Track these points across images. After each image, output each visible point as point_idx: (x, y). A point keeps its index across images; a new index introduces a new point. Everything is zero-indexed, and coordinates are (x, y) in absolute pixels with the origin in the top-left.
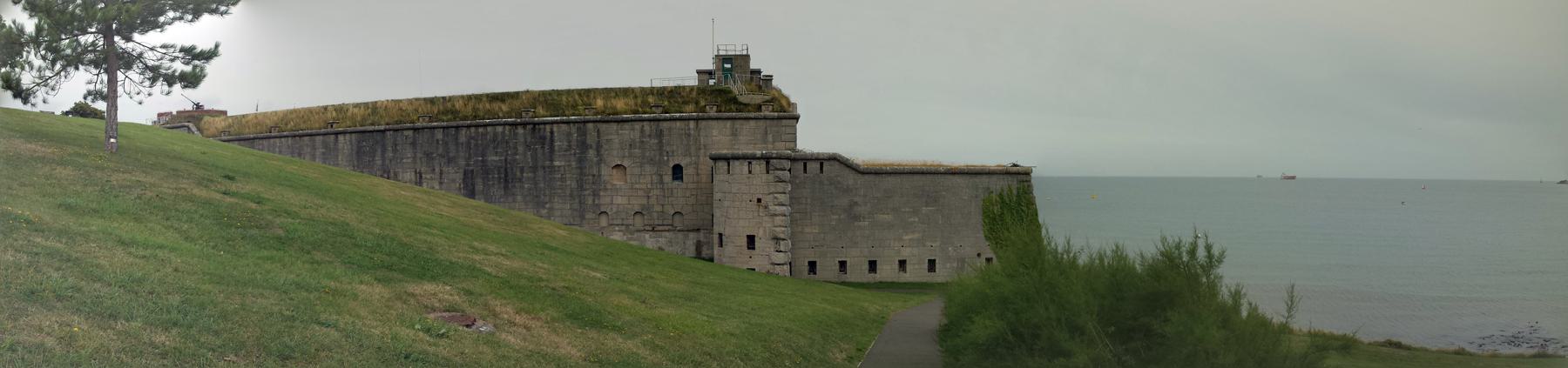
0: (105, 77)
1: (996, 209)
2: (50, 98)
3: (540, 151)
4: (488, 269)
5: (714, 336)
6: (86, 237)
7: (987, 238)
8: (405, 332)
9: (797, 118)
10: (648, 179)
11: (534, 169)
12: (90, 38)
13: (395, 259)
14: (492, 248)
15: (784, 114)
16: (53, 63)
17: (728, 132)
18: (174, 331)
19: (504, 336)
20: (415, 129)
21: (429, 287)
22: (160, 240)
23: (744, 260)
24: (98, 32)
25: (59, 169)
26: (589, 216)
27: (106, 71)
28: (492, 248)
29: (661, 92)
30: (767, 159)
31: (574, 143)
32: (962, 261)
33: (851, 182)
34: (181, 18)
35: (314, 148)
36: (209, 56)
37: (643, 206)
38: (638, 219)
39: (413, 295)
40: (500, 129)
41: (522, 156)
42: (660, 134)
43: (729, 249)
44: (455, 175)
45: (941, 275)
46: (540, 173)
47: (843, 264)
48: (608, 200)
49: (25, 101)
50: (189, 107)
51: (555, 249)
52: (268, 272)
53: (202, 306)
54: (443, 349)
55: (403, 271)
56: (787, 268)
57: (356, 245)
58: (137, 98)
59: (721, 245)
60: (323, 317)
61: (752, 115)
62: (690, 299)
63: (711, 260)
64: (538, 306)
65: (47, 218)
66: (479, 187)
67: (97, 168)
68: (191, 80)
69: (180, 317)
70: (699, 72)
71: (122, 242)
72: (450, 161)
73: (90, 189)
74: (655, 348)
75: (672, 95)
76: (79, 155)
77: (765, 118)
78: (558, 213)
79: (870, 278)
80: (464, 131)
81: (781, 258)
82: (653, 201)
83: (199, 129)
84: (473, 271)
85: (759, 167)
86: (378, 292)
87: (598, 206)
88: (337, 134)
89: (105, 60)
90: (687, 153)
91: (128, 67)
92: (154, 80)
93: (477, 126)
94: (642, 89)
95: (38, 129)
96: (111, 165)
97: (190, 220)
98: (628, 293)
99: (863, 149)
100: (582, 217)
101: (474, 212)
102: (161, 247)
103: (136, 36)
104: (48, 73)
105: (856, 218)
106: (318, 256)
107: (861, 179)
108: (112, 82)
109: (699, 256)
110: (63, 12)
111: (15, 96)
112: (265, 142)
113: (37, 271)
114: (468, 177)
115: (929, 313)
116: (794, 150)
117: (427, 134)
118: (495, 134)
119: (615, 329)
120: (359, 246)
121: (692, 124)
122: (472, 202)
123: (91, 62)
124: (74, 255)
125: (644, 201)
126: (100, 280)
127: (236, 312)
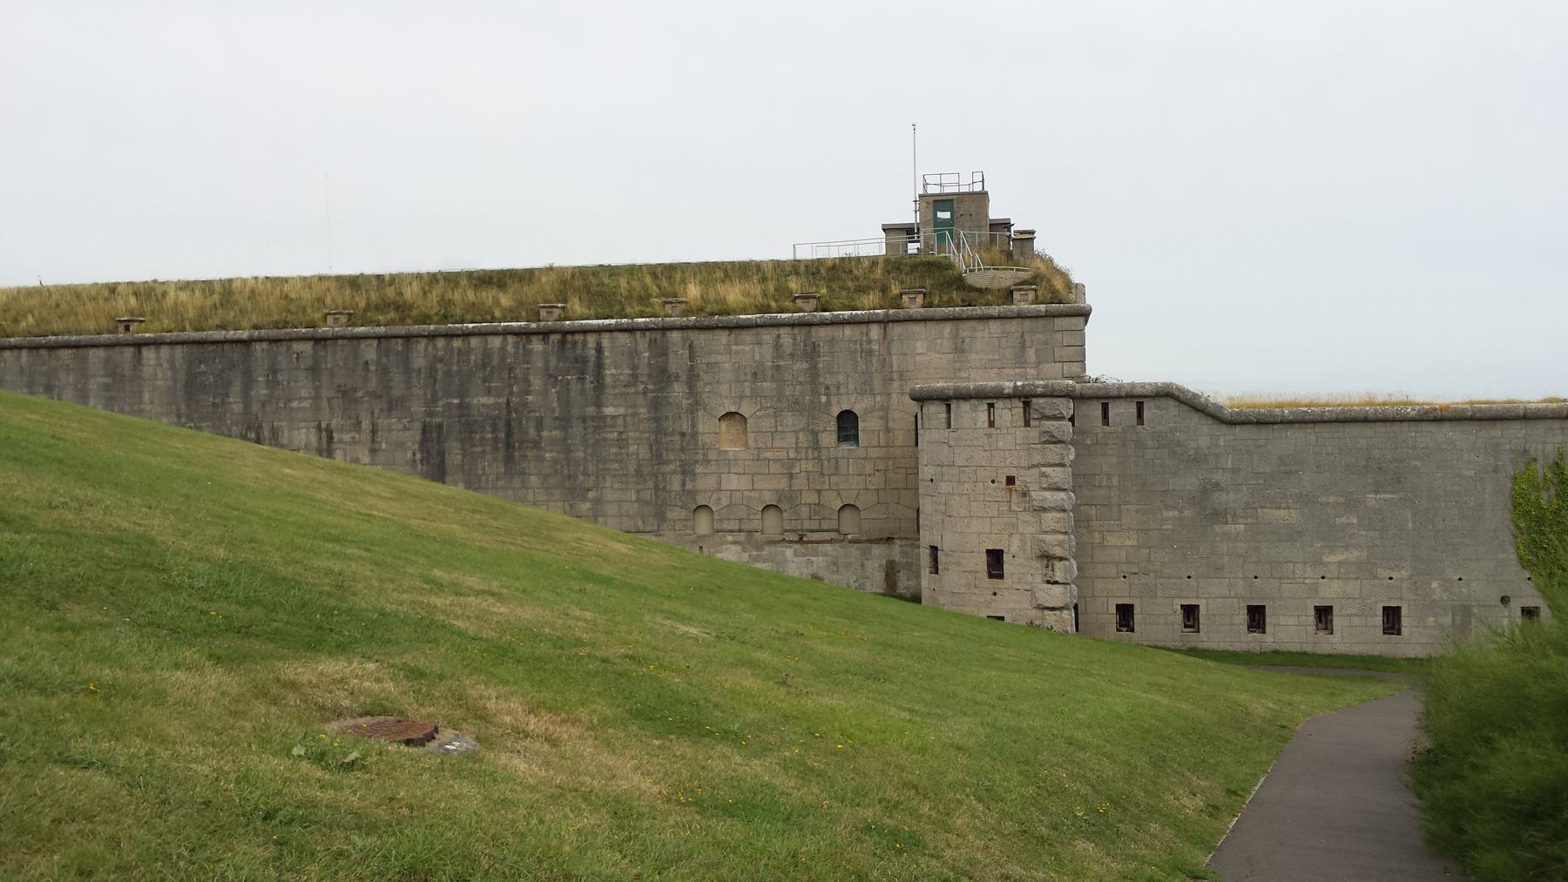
1: (1546, 498)
3: (575, 387)
5: (922, 750)
7: (1524, 563)
8: (271, 765)
9: (1085, 314)
11: (564, 422)
13: (257, 611)
14: (473, 581)
15: (1059, 306)
17: (947, 345)
19: (504, 759)
20: (318, 340)
21: (331, 666)
23: (982, 599)
26: (674, 514)
29: (813, 270)
30: (1025, 398)
31: (643, 370)
32: (1464, 612)
33: (1204, 442)
35: (84, 374)
38: (771, 519)
39: (293, 685)
40: (496, 342)
41: (539, 395)
42: (812, 352)
43: (952, 577)
44: (402, 433)
45: (1414, 640)
46: (577, 429)
47: (1190, 612)
48: (711, 482)
51: (608, 582)
54: (352, 794)
55: (274, 636)
56: (1068, 616)
57: (167, 586)
60: (76, 748)
61: (994, 310)
63: (916, 599)
66: (454, 458)
72: (393, 405)
74: (806, 773)
75: (834, 277)
77: (1021, 316)
78: (612, 509)
79: (1250, 641)
81: (1056, 596)
82: (800, 483)
84: (428, 629)
85: (1009, 414)
88: (139, 345)
90: (866, 389)
93: (450, 336)
94: (777, 265)
99: (1227, 374)
100: (661, 517)
101: (444, 508)
105: (1218, 516)
106: (75, 613)
107: (1226, 436)
109: (891, 590)
115: (1392, 724)
116: (1080, 378)
117: (342, 350)
118: (487, 354)
119: (732, 738)
121: (875, 331)
125: (783, 484)
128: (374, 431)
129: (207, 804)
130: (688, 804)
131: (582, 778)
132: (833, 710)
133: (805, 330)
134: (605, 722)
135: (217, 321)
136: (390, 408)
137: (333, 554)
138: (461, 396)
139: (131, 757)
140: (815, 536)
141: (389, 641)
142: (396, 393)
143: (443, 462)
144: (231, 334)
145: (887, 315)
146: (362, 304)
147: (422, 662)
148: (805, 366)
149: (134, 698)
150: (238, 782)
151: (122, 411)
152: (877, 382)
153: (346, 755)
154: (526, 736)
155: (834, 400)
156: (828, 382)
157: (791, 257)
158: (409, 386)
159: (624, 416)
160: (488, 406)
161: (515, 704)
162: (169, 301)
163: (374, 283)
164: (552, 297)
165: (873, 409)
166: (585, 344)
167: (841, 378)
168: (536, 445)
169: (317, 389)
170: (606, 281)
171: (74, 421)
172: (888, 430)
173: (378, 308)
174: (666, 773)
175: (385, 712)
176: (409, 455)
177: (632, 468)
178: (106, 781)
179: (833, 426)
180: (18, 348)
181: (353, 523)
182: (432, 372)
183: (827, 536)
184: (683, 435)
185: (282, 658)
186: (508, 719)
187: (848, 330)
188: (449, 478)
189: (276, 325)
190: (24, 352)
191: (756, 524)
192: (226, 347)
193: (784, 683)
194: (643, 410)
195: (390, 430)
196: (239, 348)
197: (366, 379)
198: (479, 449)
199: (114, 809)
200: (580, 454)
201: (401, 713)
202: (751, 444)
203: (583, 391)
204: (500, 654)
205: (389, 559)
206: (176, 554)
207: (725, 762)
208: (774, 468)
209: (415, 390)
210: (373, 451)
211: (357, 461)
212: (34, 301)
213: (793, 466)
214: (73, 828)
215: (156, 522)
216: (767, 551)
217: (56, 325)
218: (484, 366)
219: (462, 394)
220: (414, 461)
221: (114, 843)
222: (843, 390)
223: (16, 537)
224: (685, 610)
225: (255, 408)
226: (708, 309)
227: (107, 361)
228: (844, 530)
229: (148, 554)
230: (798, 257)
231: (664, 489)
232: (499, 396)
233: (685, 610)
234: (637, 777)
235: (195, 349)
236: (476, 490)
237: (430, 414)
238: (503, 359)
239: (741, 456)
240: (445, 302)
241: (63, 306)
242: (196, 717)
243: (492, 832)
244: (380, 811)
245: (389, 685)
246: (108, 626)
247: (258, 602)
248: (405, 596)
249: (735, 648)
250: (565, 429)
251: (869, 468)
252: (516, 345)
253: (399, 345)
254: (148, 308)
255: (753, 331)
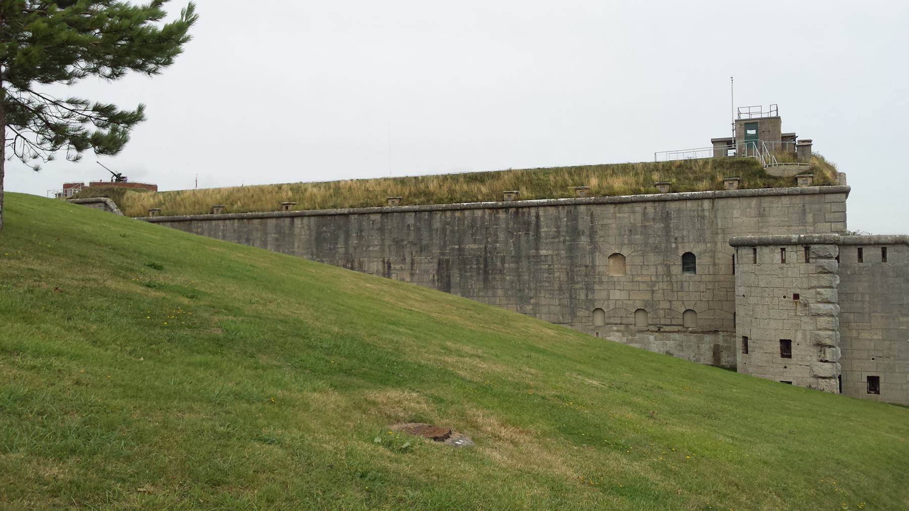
3: (523, 238)
9: (846, 192)
10: (652, 270)
11: (517, 259)
14: (468, 349)
15: (830, 187)
17: (754, 212)
18: (71, 461)
20: (383, 213)
21: (394, 394)
22: (57, 345)
26: (581, 313)
28: (468, 349)
29: (667, 168)
30: (806, 245)
31: (563, 229)
34: (95, 71)
35: (265, 233)
37: (646, 302)
38: (640, 317)
39: (374, 403)
40: (479, 213)
41: (503, 243)
42: (666, 218)
43: (756, 356)
44: (428, 265)
46: (524, 263)
48: (604, 294)
50: (107, 178)
53: (111, 427)
55: (364, 376)
56: (835, 383)
57: (309, 346)
58: (33, 163)
59: (746, 350)
60: (265, 432)
61: (785, 190)
62: (709, 415)
63: (733, 369)
64: (526, 418)
66: (456, 279)
68: (110, 145)
69: (80, 442)
70: (714, 142)
72: (422, 249)
75: (682, 171)
77: (803, 194)
78: (544, 310)
81: (826, 369)
82: (659, 296)
83: (119, 206)
84: (445, 375)
85: (795, 255)
86: (332, 400)
87: (592, 301)
88: (293, 217)
90: (701, 239)
92: (57, 142)
93: (454, 210)
94: (645, 165)
97: (101, 320)
98: (630, 404)
100: (573, 314)
101: (449, 307)
102: (59, 354)
106: (263, 360)
109: (717, 363)
112: (205, 225)
114: (443, 267)
116: (843, 232)
117: (396, 218)
118: (474, 220)
121: (707, 204)
122: (449, 297)
125: (648, 297)
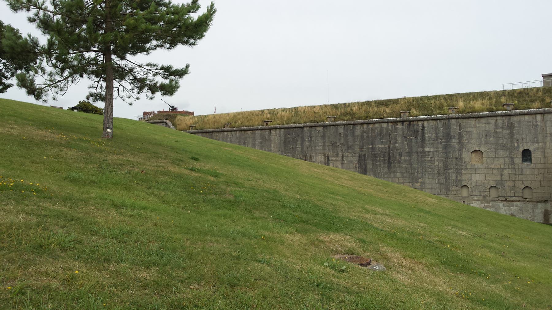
0: (104, 84)
2: (59, 97)
3: (414, 141)
4: (376, 225)
6: (86, 202)
8: (317, 268)
10: (502, 161)
11: (410, 153)
12: (93, 55)
13: (310, 216)
14: (379, 210)
16: (62, 70)
18: (154, 269)
19: (395, 274)
20: (324, 126)
21: (334, 236)
22: (144, 203)
24: (99, 51)
25: (65, 151)
26: (453, 188)
27: (105, 80)
28: (379, 210)
29: (511, 94)
31: (440, 135)
34: (161, 46)
35: (254, 139)
36: (181, 73)
39: (323, 242)
40: (385, 125)
41: (401, 144)
42: (511, 126)
44: (352, 158)
46: (414, 156)
48: (468, 176)
49: (38, 97)
50: (167, 109)
51: (428, 213)
52: (222, 225)
53: (174, 250)
54: (344, 281)
55: (316, 225)
57: (283, 206)
58: (128, 101)
60: (260, 256)
64: (419, 254)
65: (54, 188)
66: (370, 166)
67: (97, 151)
71: (115, 205)
73: (90, 166)
74: (515, 292)
75: (522, 96)
76: (82, 140)
78: (428, 186)
80: (359, 127)
82: (506, 177)
83: (174, 124)
84: (366, 226)
88: (270, 129)
89: (104, 72)
90: (535, 140)
91: (122, 77)
92: (141, 89)
93: (368, 124)
94: (496, 93)
95: (50, 120)
96: (108, 148)
97: (167, 189)
98: (491, 249)
100: (448, 189)
102: (145, 208)
103: (128, 56)
104: (58, 78)
106: (257, 214)
108: (109, 88)
110: (71, 33)
111: (29, 93)
113: (45, 229)
114: (362, 159)
117: (332, 129)
118: (381, 130)
119: (480, 274)
120: (285, 207)
122: (364, 177)
123: (93, 72)
124: (77, 216)
125: (498, 178)
126: (97, 233)
127: (199, 254)
128: (343, 157)
129: (299, 279)
130: (466, 298)
131: (424, 284)
132: (525, 268)
133: (508, 118)
134: (431, 265)
135: (293, 121)
136: (348, 149)
137: (332, 198)
138: (372, 145)
139: (276, 261)
140: (512, 199)
141: (352, 229)
142: (350, 144)
143: (366, 167)
144: (298, 125)
145: (544, 111)
146: (339, 114)
147: (364, 237)
148: (508, 131)
149: (275, 242)
150: (308, 272)
151: (265, 150)
152: (540, 138)
153: (341, 267)
154: (403, 267)
155: (521, 145)
156: (518, 138)
157: (501, 89)
158: (354, 141)
159: (433, 152)
160: (382, 148)
161: (398, 255)
162: (279, 115)
163: (343, 106)
164: (405, 109)
165: (538, 148)
166: (418, 125)
167: (524, 136)
168: (399, 162)
169: (324, 143)
170: (426, 102)
171: (251, 153)
172: (545, 157)
173: (344, 115)
174: (457, 286)
175: (352, 253)
176: (354, 165)
177: (436, 171)
178: (269, 268)
179: (520, 155)
180: (236, 131)
181: (338, 188)
182: (362, 136)
183: (517, 199)
184: (456, 158)
185: (318, 232)
186: (395, 260)
187: (527, 117)
188: (368, 173)
189: (311, 122)
190: (238, 132)
191: (487, 193)
192: (296, 129)
193: (503, 256)
194: (440, 149)
195: (348, 157)
196: (300, 129)
197: (340, 139)
198: (378, 163)
199: (272, 277)
200: (416, 165)
201: (358, 254)
202: (485, 162)
203: (417, 143)
204: (391, 236)
205: (351, 201)
206: (285, 196)
207: (480, 284)
208: (495, 172)
209: (356, 143)
210: (342, 164)
211: (337, 167)
212: (240, 117)
213: (503, 171)
214: (260, 282)
215: (278, 186)
216: (491, 204)
217: (247, 124)
218: (380, 134)
219: (373, 144)
220: (356, 167)
221: (272, 288)
222: (524, 141)
223: (239, 189)
224: (460, 225)
225: (305, 149)
226: (467, 111)
227: (261, 135)
228: (525, 196)
229: (277, 196)
230: (505, 89)
231: (449, 179)
232: (385, 144)
233: (460, 225)
234: (445, 287)
235: (286, 130)
236: (378, 178)
237: (362, 151)
238: (387, 131)
239: (481, 167)
240: (367, 112)
241: (249, 117)
242: (293, 250)
243: (393, 300)
244: (354, 288)
245: (354, 244)
246: (266, 218)
247: (310, 213)
248: (357, 214)
249: (482, 241)
250: (410, 156)
251: (536, 172)
252: (392, 126)
253: (351, 127)
254: (273, 117)
255: (486, 119)
